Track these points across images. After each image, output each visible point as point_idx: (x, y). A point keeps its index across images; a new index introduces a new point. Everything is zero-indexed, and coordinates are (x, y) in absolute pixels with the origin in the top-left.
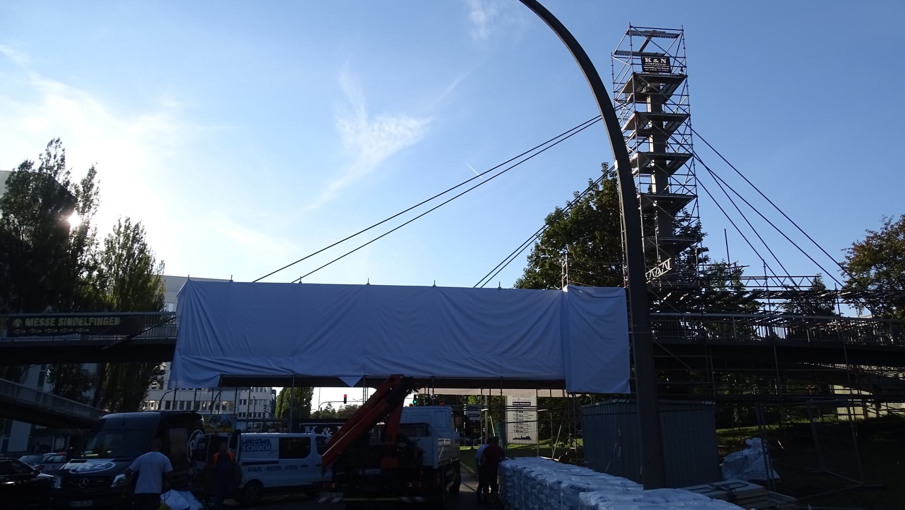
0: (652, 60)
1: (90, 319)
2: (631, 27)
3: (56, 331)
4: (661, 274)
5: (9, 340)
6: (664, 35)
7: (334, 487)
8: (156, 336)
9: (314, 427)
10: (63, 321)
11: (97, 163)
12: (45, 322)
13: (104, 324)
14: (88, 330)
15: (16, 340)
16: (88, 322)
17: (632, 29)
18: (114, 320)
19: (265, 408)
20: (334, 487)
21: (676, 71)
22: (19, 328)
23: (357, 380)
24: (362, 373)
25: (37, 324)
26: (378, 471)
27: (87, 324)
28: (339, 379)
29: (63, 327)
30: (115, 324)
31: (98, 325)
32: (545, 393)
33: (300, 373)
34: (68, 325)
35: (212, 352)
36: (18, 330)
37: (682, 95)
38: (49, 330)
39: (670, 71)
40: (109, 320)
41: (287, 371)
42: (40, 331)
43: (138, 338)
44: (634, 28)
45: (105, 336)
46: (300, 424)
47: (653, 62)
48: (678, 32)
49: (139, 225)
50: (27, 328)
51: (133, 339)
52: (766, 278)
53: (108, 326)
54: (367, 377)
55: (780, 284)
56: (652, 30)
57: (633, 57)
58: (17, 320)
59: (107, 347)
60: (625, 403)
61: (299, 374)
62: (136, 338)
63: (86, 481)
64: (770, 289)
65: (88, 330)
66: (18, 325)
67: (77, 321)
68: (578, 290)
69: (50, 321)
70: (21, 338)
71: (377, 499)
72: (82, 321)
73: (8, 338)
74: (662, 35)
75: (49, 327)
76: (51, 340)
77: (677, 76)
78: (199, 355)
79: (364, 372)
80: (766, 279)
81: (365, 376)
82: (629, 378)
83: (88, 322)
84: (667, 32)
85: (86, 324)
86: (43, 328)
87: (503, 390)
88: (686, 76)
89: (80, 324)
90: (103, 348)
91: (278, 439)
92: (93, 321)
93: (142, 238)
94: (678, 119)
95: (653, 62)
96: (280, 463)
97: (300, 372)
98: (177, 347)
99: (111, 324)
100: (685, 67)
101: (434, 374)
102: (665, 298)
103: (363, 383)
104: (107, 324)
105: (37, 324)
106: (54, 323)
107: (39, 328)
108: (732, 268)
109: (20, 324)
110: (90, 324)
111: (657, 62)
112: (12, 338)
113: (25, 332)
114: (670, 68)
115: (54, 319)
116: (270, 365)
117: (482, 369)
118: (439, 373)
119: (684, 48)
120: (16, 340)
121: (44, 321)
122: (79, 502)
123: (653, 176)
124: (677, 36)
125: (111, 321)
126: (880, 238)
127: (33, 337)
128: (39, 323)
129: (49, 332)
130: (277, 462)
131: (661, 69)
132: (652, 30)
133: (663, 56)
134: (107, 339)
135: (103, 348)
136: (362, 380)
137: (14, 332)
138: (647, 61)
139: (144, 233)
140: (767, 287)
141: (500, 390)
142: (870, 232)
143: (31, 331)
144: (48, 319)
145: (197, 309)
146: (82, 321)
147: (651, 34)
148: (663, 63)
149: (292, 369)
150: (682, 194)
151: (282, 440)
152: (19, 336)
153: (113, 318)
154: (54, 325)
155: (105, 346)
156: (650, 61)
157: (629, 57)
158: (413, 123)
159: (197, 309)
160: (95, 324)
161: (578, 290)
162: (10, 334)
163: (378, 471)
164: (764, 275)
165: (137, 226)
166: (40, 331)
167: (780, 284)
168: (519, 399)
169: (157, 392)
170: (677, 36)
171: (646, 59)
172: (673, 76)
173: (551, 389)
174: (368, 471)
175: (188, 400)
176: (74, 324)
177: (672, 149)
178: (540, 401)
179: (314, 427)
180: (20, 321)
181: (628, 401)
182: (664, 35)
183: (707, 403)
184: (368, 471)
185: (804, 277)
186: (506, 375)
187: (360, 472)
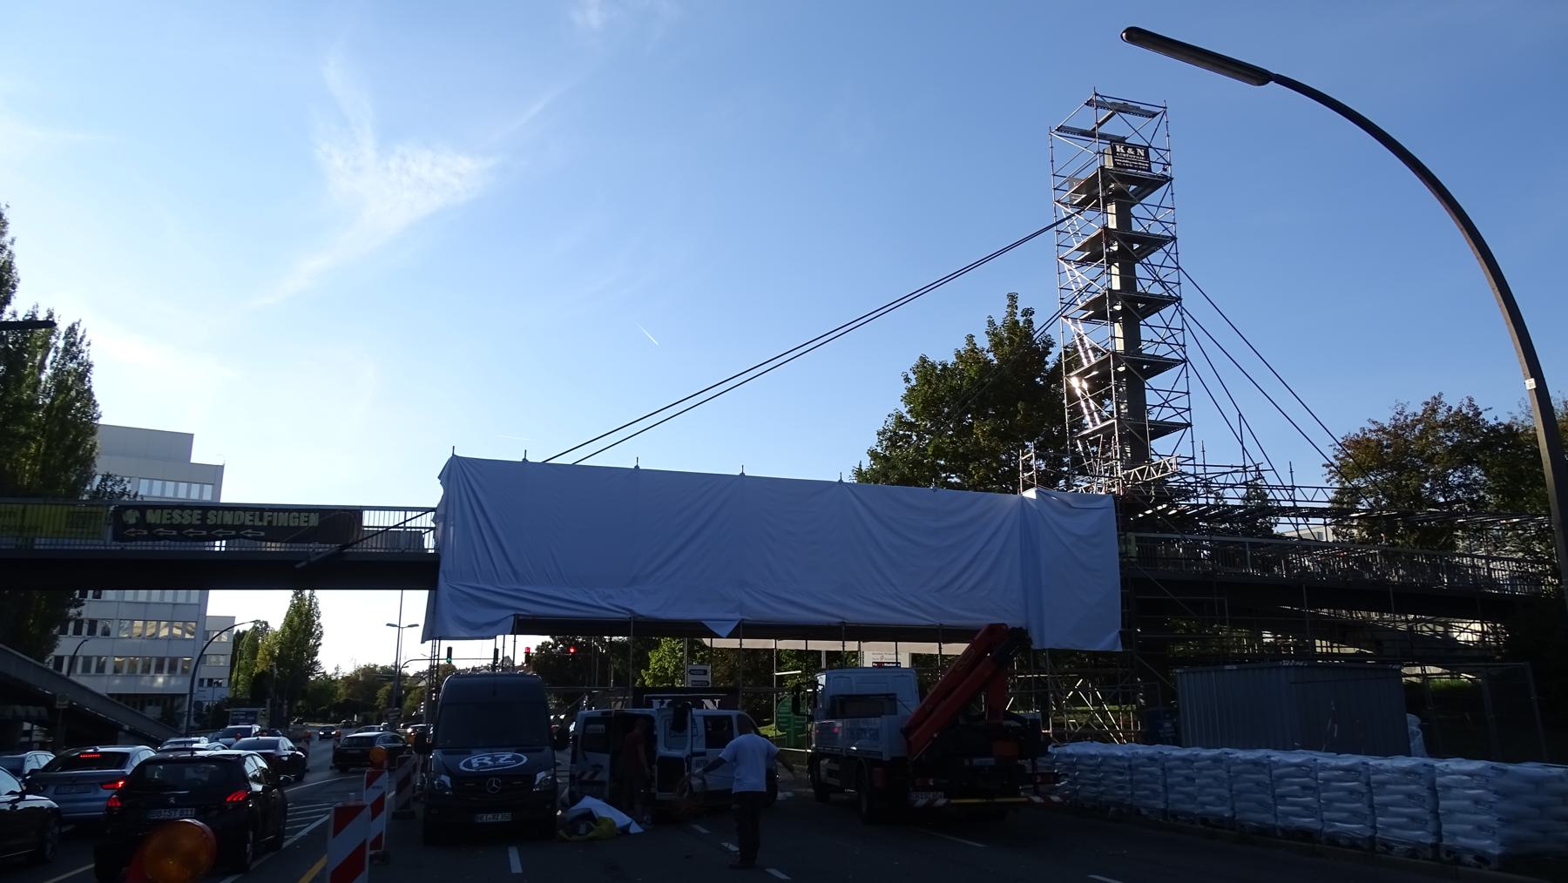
0: (1126, 149)
1: (266, 514)
2: (1096, 94)
3: (204, 533)
4: (1156, 477)
5: (116, 546)
6: (1137, 112)
7: (931, 784)
8: (383, 546)
9: (667, 701)
10: (216, 516)
11: (7, 206)
12: (183, 518)
13: (292, 524)
14: (262, 534)
15: (131, 546)
16: (261, 519)
17: (1098, 98)
18: (308, 517)
19: (117, 670)
20: (931, 784)
21: (1157, 170)
22: (135, 526)
23: (731, 627)
24: (738, 616)
25: (168, 519)
26: (991, 761)
27: (260, 524)
28: (703, 625)
29: (216, 526)
30: (311, 525)
31: (280, 525)
32: (930, 648)
33: (642, 614)
34: (224, 523)
35: (497, 575)
36: (133, 530)
37: (1159, 207)
38: (191, 530)
39: (1149, 170)
40: (299, 518)
41: (624, 611)
42: (175, 533)
43: (355, 550)
44: (1102, 96)
45: (294, 545)
46: (645, 696)
47: (1126, 153)
48: (1158, 110)
49: (76, 327)
50: (150, 527)
51: (346, 550)
52: (1293, 488)
53: (298, 528)
54: (745, 622)
55: (1287, 498)
56: (1122, 102)
57: (1101, 141)
58: (130, 512)
59: (303, 564)
60: (1303, 666)
61: (642, 616)
62: (351, 550)
63: (497, 783)
64: (1299, 505)
65: (262, 534)
66: (132, 521)
67: (242, 517)
68: (1050, 496)
69: (191, 516)
70: (139, 543)
71: (985, 801)
72: (252, 518)
73: (114, 543)
74: (1134, 111)
75: (190, 526)
76: (149, 548)
77: (1159, 177)
78: (478, 583)
79: (741, 614)
80: (1293, 490)
81: (743, 620)
82: (1120, 629)
83: (261, 519)
84: (1142, 107)
85: (257, 523)
86: (180, 527)
87: (743, 640)
88: (1171, 179)
89: (248, 523)
90: (298, 566)
91: (702, 718)
92: (270, 518)
93: (80, 352)
94: (1152, 243)
95: (1126, 153)
96: (707, 754)
97: (643, 612)
98: (442, 567)
99: (303, 524)
100: (1170, 165)
101: (844, 618)
102: (1149, 512)
103: (523, 626)
104: (296, 524)
105: (168, 519)
106: (198, 520)
107: (171, 526)
108: (1250, 471)
109: (137, 518)
110: (265, 524)
111: (1132, 153)
112: (123, 544)
113: (145, 532)
114: (1149, 164)
115: (200, 512)
116: (595, 601)
117: (914, 612)
118: (852, 617)
119: (1168, 136)
120: (131, 546)
121: (181, 516)
122: (490, 816)
123: (1117, 325)
124: (1154, 115)
125: (303, 518)
126: (1383, 429)
127: (162, 543)
128: (172, 517)
129: (191, 535)
130: (703, 754)
131: (1134, 165)
132: (1122, 102)
133: (1141, 147)
134: (297, 550)
135: (298, 566)
136: (738, 626)
137: (125, 533)
138: (1118, 150)
139: (84, 343)
140: (1294, 501)
141: (739, 640)
142: (1374, 422)
143: (158, 532)
144: (188, 511)
145: (470, 503)
146: (252, 518)
147: (1123, 108)
148: (1141, 156)
149: (631, 608)
150: (1153, 355)
151: (739, 716)
152: (135, 539)
153: (307, 514)
154: (199, 522)
155: (301, 561)
156: (1123, 151)
157: (1093, 140)
158: (465, 164)
159: (470, 503)
160: (275, 524)
161: (1050, 496)
162: (118, 536)
163: (991, 761)
164: (1291, 484)
165: (72, 330)
166: (175, 533)
167: (1287, 498)
168: (882, 658)
169: (70, 639)
170: (1154, 115)
171: (1118, 147)
172: (1154, 176)
173: (896, 641)
174: (976, 761)
175: (158, 655)
176: (236, 523)
177: (1146, 285)
178: (915, 658)
179: (667, 701)
180: (137, 514)
181: (1306, 665)
182: (1137, 112)
183: (1394, 667)
184: (976, 761)
185: (1318, 488)
186: (948, 622)
187: (967, 763)
